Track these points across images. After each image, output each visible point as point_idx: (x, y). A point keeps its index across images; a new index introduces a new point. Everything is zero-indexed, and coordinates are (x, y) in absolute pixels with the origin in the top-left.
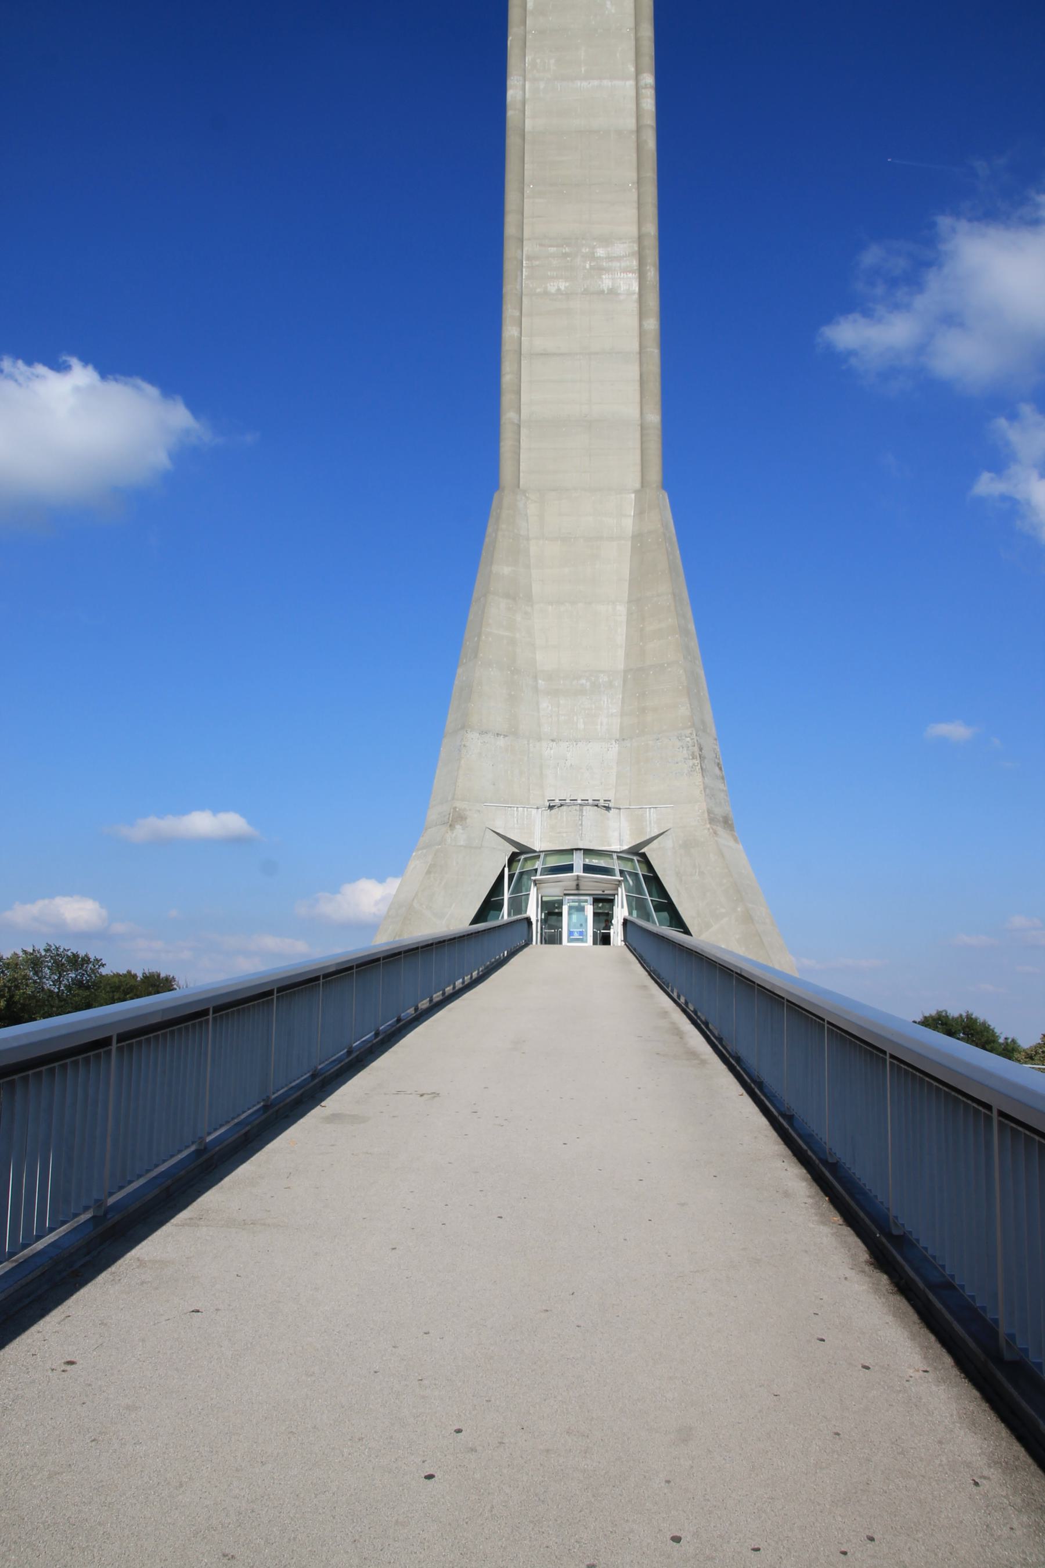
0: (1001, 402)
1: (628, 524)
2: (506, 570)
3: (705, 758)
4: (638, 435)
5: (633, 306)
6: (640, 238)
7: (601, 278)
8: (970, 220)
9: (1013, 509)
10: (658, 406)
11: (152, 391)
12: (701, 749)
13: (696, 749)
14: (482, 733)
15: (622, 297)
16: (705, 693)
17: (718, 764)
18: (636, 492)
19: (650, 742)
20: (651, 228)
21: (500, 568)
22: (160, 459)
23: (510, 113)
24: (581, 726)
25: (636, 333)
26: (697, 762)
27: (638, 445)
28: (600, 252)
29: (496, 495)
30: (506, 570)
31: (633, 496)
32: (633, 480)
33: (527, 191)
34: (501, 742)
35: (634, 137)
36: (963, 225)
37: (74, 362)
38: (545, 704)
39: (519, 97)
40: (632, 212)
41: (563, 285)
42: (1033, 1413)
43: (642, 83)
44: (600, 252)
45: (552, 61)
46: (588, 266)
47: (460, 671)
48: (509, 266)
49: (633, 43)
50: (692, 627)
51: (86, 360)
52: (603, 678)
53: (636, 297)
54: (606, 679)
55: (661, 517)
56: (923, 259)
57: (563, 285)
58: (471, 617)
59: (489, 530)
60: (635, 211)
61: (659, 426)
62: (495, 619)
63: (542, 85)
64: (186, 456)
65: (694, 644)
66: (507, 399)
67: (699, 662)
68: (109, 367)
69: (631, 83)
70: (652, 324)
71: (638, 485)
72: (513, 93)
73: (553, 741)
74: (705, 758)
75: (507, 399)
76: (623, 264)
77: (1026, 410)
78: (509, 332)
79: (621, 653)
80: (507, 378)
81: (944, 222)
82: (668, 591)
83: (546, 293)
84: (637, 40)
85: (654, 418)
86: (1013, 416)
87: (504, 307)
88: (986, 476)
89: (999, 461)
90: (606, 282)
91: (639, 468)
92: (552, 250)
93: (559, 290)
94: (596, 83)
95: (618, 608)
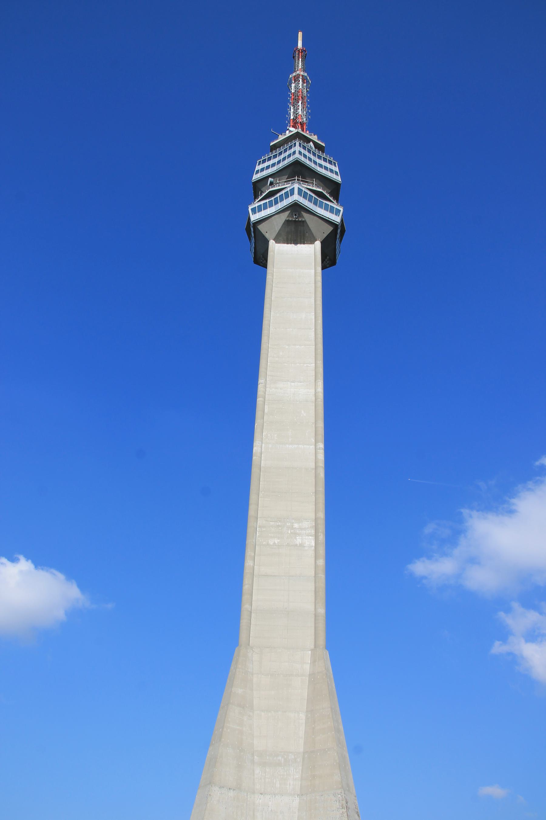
0: (502, 603)
1: (307, 667)
2: (240, 691)
3: (349, 808)
4: (313, 620)
5: (312, 553)
6: (316, 519)
7: (296, 538)
8: (478, 511)
9: (513, 660)
10: (324, 605)
11: (61, 576)
12: (347, 803)
13: (344, 802)
14: (221, 787)
15: (306, 548)
16: (349, 767)
17: (357, 812)
18: (312, 650)
19: (318, 797)
20: (322, 515)
21: (236, 690)
22: (61, 614)
23: (254, 458)
24: (278, 785)
25: (313, 567)
26: (344, 810)
27: (313, 625)
28: (296, 525)
29: (237, 649)
30: (240, 691)
31: (310, 652)
32: (310, 643)
33: (261, 495)
34: (231, 793)
35: (314, 471)
36: (475, 513)
37: (22, 558)
38: (258, 771)
39: (259, 451)
40: (312, 507)
41: (276, 541)
42: (299, 42)
43: (318, 447)
44: (296, 525)
45: (276, 435)
46: (289, 532)
47: (211, 748)
48: (250, 530)
49: (314, 429)
50: (341, 727)
51: (27, 558)
52: (291, 757)
53: (313, 548)
54: (293, 757)
55: (325, 664)
56: (457, 532)
57: (276, 541)
58: (219, 717)
59: (232, 668)
60: (314, 506)
61: (324, 615)
62: (232, 719)
63: (270, 446)
64: (74, 613)
65: (343, 738)
66: (245, 597)
67: (345, 748)
68: (40, 561)
69: (313, 447)
70: (321, 562)
71: (312, 647)
72: (256, 449)
73: (261, 794)
74: (349, 808)
75: (245, 597)
76: (307, 532)
77: (515, 605)
78: (248, 563)
79: (302, 742)
80: (246, 587)
81: (465, 512)
82: (328, 706)
83: (268, 544)
84: (316, 427)
85: (322, 611)
86: (508, 610)
87: (246, 551)
88: (497, 643)
89: (504, 634)
90: (298, 541)
91: (313, 637)
92: (272, 523)
93: (274, 543)
94: (296, 446)
95: (301, 715)
